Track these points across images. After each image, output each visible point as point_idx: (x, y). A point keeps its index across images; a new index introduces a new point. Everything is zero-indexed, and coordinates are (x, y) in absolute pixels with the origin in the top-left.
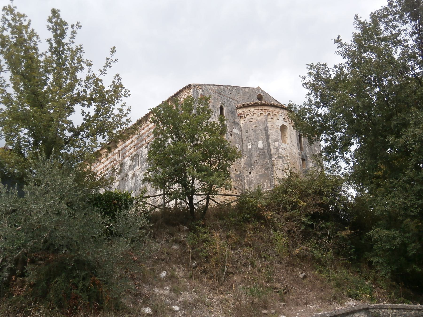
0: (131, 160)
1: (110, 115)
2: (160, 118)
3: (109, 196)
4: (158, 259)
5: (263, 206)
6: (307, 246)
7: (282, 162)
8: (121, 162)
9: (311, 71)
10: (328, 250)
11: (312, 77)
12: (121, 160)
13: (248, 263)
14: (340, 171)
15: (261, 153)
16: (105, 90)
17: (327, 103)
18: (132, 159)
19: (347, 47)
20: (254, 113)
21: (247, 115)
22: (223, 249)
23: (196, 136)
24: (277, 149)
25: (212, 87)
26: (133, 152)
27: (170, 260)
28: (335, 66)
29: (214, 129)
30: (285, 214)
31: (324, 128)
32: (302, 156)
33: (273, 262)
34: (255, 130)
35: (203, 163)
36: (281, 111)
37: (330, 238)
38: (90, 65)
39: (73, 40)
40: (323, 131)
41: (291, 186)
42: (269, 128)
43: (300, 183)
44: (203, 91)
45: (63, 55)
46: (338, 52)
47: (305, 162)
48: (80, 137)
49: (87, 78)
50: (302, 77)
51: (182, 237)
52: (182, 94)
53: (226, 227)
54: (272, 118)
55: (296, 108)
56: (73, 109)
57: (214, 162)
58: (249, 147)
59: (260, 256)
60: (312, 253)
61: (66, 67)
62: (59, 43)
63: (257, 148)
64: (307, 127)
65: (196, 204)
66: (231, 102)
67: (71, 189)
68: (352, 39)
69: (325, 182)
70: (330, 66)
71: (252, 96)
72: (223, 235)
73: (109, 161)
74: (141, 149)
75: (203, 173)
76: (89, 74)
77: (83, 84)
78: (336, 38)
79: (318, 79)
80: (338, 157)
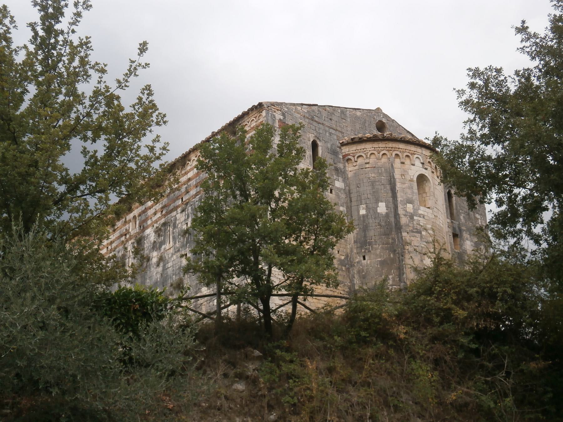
0: (156, 232)
1: (132, 157)
2: (214, 161)
3: (125, 295)
4: (210, 407)
5: (390, 316)
6: (468, 388)
7: (419, 239)
8: (138, 237)
9: (475, 82)
10: (506, 396)
11: (475, 91)
12: (138, 233)
13: (366, 416)
14: (524, 256)
15: (383, 224)
16: (125, 112)
17: (501, 137)
18: (158, 232)
19: (538, 41)
20: (372, 154)
21: (358, 157)
22: (322, 391)
23: (276, 193)
24: (412, 217)
25: (299, 108)
26: (160, 219)
27: (231, 408)
28: (517, 73)
29: (307, 181)
30: (430, 331)
31: (495, 181)
32: (454, 229)
33: (409, 415)
34: (373, 184)
35: (287, 241)
36: (419, 150)
37: (508, 374)
38: (103, 71)
39: (74, 27)
40: (494, 186)
41: (440, 282)
42: (397, 180)
43: (455, 275)
44: (283, 114)
45: (55, 52)
46: (522, 49)
47: (459, 239)
48: (79, 194)
49: (95, 92)
50: (458, 91)
51: (251, 368)
52: (246, 121)
53: (327, 353)
54: (403, 163)
55: (446, 145)
56: (68, 144)
57: (306, 239)
58: (363, 212)
59: (387, 404)
60: (477, 400)
61: (59, 73)
62: (49, 30)
63: (377, 215)
64: (463, 178)
65: (274, 311)
66: (330, 134)
67: (66, 285)
68: (549, 25)
69: (500, 276)
70: (508, 72)
71: (367, 125)
72: (322, 365)
73: (117, 234)
74: (174, 213)
75: (290, 258)
76: (99, 85)
77: (87, 102)
78: (519, 25)
79: (487, 94)
80: (520, 231)
